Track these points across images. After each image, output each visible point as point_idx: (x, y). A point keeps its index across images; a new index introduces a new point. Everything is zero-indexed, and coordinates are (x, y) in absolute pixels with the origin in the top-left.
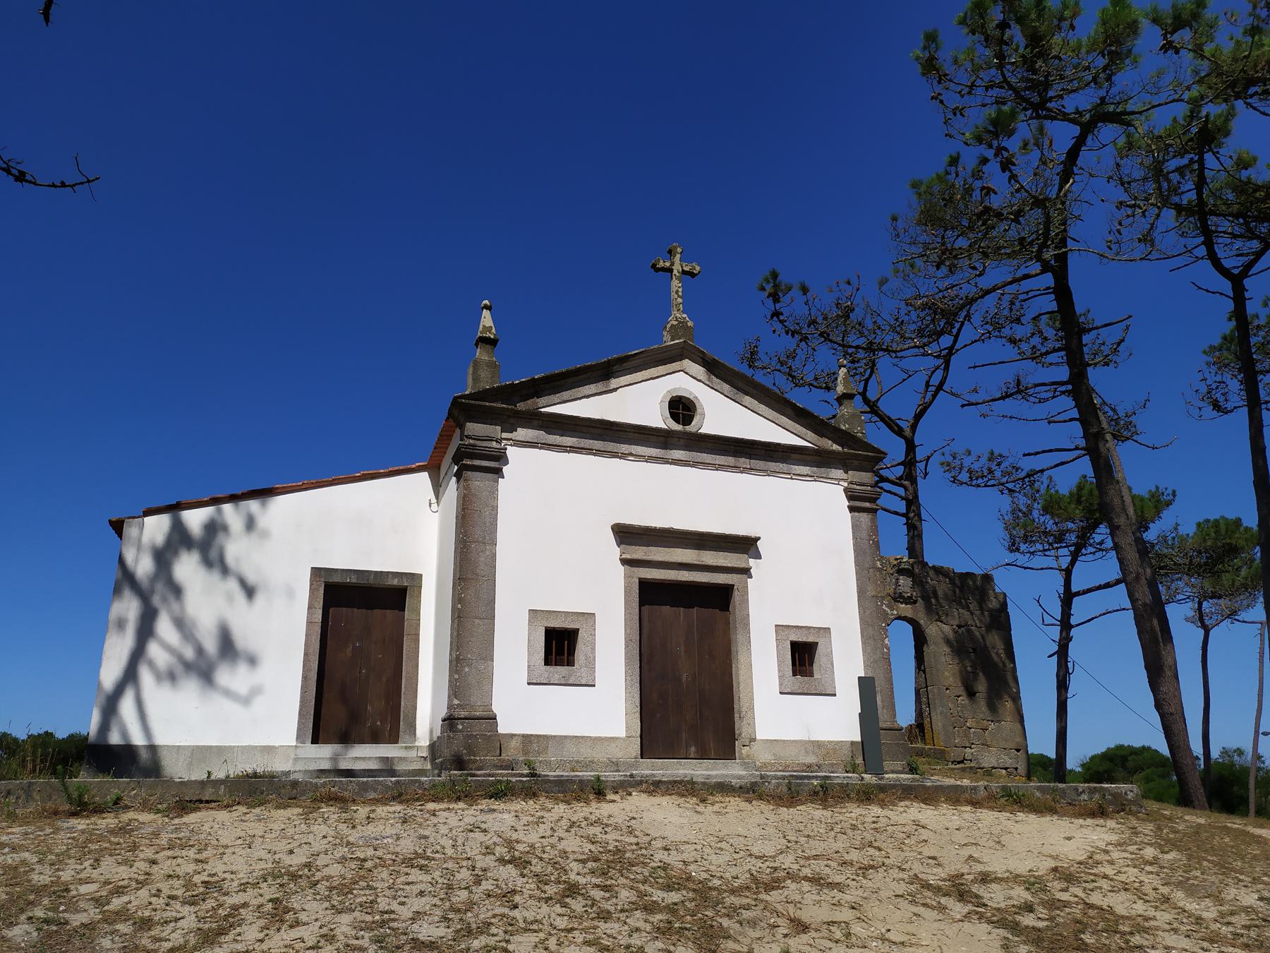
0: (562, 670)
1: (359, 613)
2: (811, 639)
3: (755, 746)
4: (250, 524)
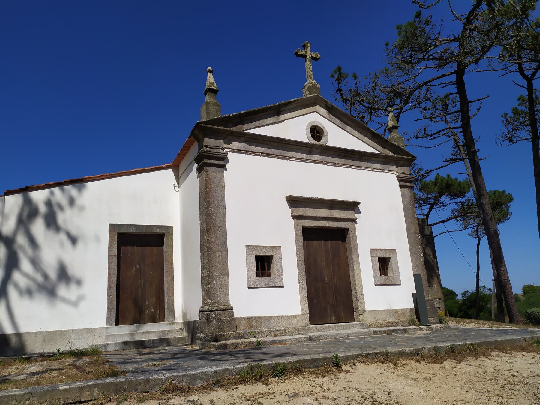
0: (265, 279)
1: (139, 251)
2: (387, 256)
3: (366, 314)
4: (72, 202)
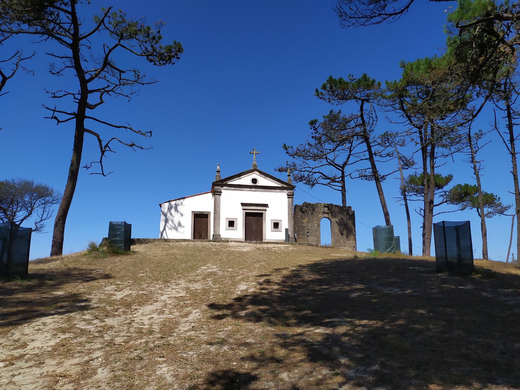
1: (200, 219)
4: (182, 204)
